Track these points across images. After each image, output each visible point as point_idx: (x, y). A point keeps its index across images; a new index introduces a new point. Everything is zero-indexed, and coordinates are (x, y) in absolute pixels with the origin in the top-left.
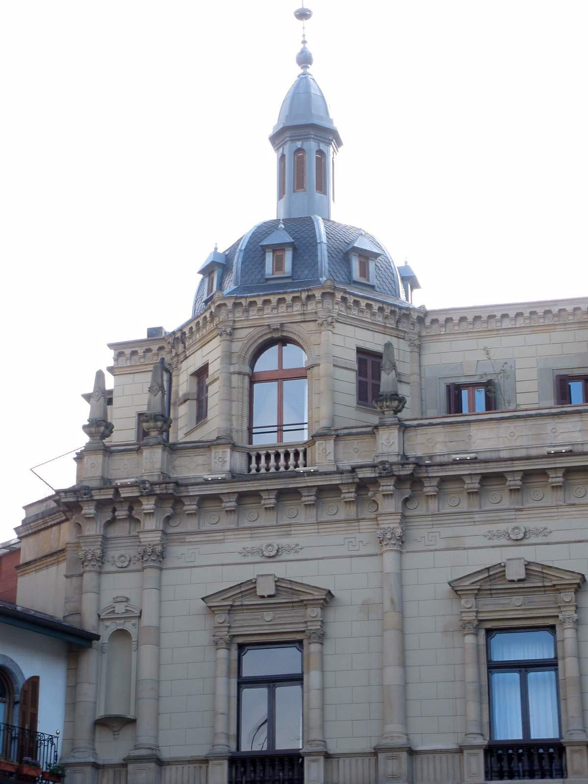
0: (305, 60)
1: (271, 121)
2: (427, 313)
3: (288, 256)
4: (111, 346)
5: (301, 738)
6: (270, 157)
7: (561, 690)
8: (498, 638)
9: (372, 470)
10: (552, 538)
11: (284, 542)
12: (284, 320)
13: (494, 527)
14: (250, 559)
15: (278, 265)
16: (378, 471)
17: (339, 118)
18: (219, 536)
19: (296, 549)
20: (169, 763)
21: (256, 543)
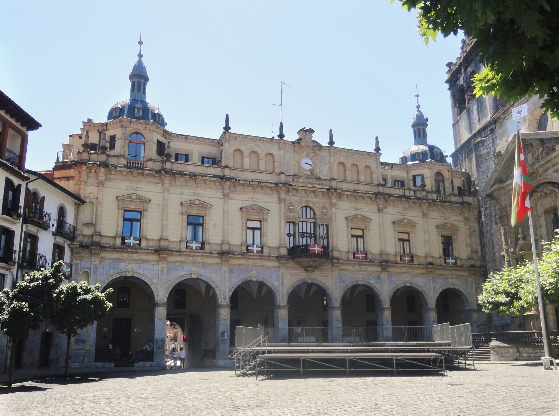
0: (140, 56)
1: (130, 70)
3: (141, 110)
4: (83, 122)
8: (126, 212)
9: (441, 217)
11: (138, 186)
13: (191, 191)
16: (495, 226)
17: (149, 73)
20: (150, 240)
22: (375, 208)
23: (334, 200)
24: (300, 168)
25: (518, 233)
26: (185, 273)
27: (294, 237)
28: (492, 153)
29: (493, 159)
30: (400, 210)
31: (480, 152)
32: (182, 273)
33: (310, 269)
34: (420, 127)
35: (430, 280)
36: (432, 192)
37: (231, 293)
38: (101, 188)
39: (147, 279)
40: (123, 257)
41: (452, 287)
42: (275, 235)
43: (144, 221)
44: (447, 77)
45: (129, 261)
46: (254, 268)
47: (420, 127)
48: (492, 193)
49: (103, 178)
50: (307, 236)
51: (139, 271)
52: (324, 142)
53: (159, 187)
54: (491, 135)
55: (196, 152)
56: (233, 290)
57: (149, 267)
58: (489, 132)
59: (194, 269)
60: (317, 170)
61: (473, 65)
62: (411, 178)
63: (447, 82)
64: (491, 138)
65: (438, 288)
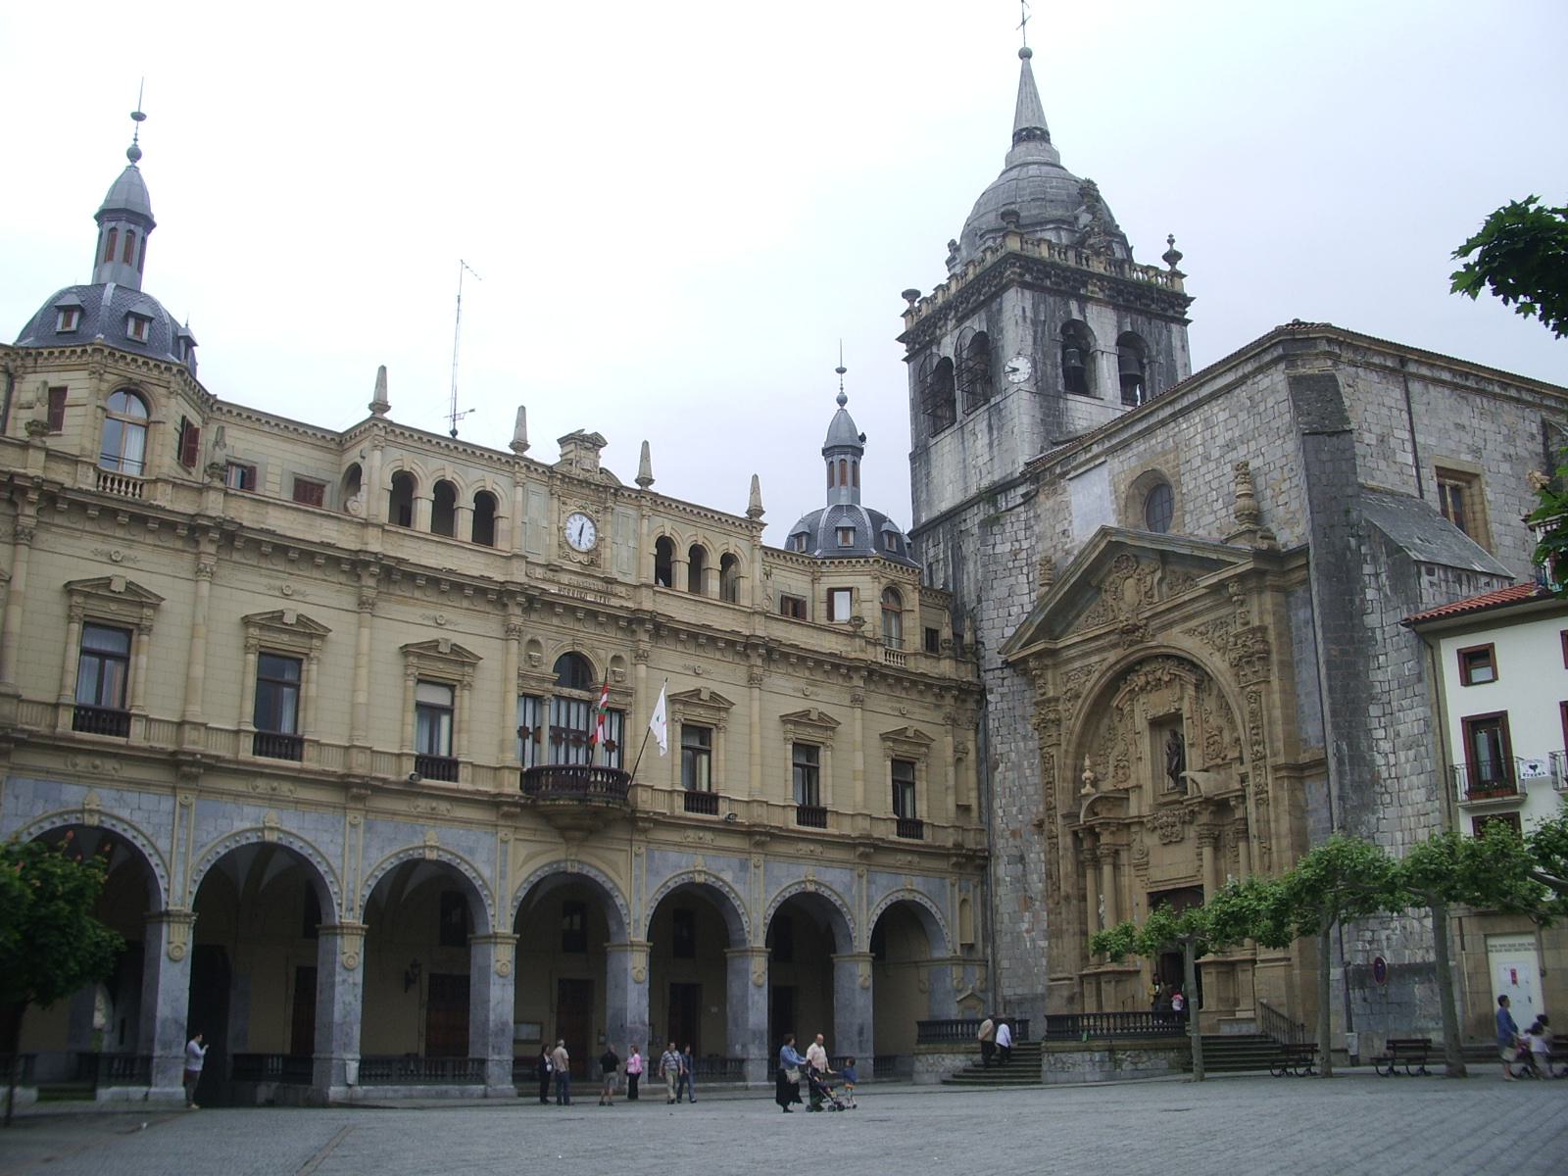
0: (134, 154)
1: (97, 202)
2: (217, 401)
3: (76, 317)
5: (1083, 696)
6: (93, 231)
7: (301, 715)
10: (307, 599)
11: (125, 552)
12: (144, 379)
14: (98, 558)
15: (68, 322)
18: (78, 534)
19: (134, 560)
21: (106, 548)
22: (741, 672)
23: (645, 645)
24: (564, 543)
25: (1083, 771)
26: (248, 825)
27: (537, 740)
28: (1023, 555)
29: (1025, 571)
30: (801, 684)
31: (994, 545)
32: (240, 825)
33: (578, 834)
34: (844, 453)
35: (860, 876)
36: (875, 643)
37: (367, 893)
38: (23, 550)
39: (140, 837)
40: (75, 765)
41: (908, 896)
42: (490, 734)
43: (141, 661)
44: (901, 327)
45: (95, 778)
46: (432, 823)
47: (844, 453)
48: (1024, 660)
49: (32, 522)
50: (567, 741)
51: (116, 812)
52: (628, 478)
53: (186, 562)
54: (1022, 508)
55: (278, 465)
56: (373, 883)
57: (148, 800)
58: (1019, 500)
59: (271, 816)
60: (607, 553)
61: (984, 316)
62: (823, 595)
63: (901, 339)
64: (1023, 517)
65: (878, 899)
